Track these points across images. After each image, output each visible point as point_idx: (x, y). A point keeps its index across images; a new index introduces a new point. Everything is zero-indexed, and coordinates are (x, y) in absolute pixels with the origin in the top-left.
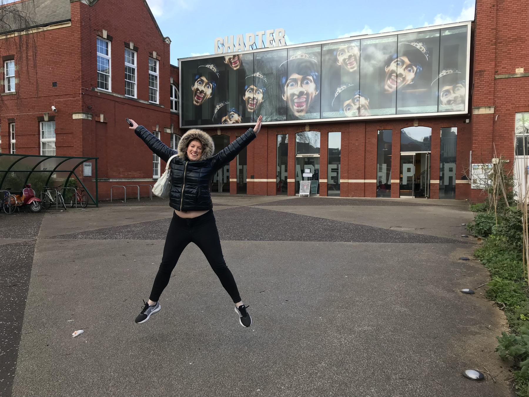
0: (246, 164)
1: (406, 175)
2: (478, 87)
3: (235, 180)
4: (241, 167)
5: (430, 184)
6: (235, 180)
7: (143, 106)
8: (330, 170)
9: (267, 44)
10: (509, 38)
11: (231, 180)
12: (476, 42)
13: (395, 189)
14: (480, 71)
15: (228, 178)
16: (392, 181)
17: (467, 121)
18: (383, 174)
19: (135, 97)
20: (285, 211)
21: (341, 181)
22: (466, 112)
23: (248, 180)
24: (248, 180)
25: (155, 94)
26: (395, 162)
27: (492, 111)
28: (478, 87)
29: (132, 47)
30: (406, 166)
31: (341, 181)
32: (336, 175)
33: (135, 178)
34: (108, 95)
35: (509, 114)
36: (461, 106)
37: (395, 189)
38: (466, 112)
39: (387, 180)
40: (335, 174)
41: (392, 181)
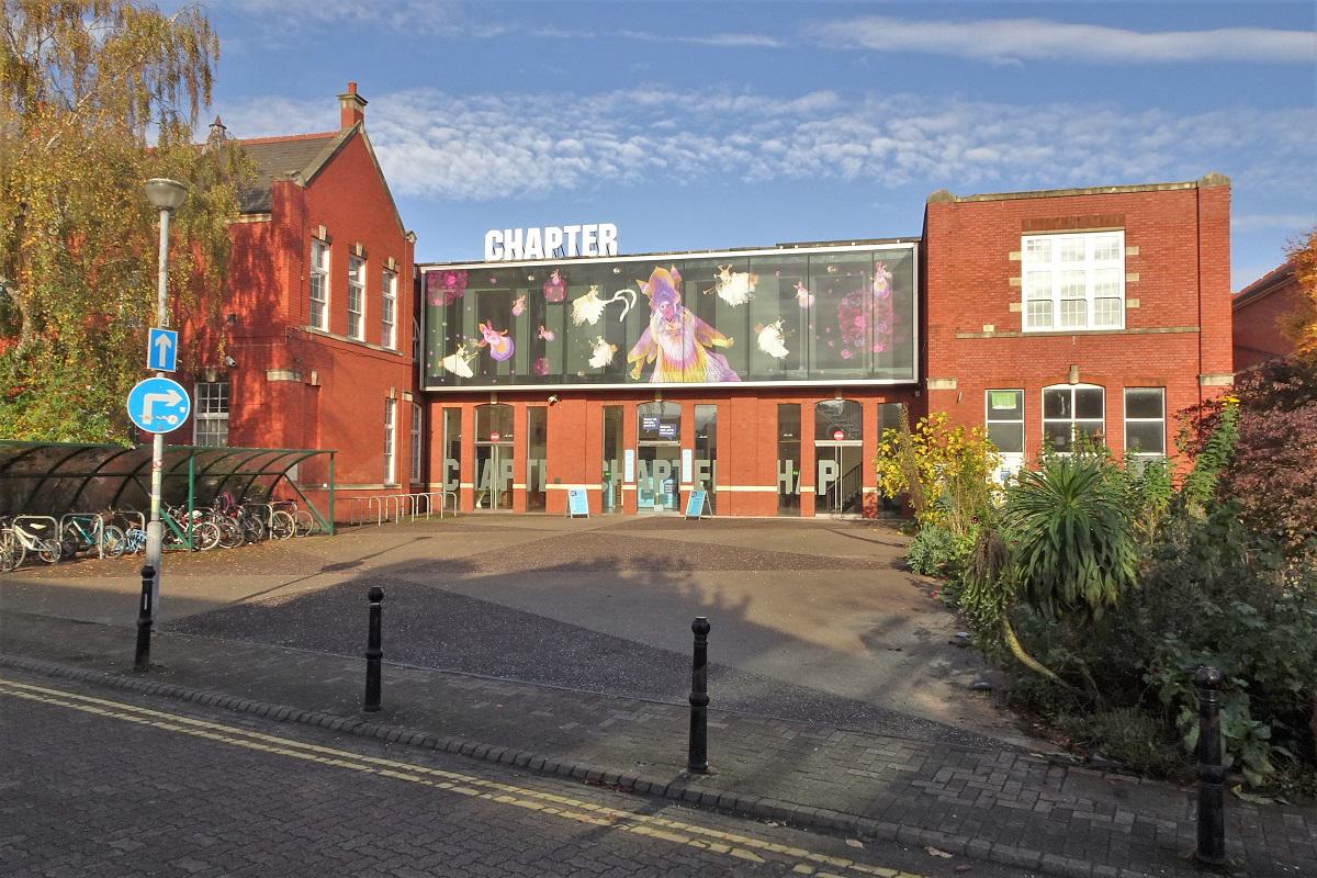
0: (545, 458)
1: (824, 478)
2: (933, 349)
3: (523, 486)
4: (532, 463)
5: (473, 482)
6: (523, 486)
7: (374, 356)
8: (698, 469)
9: (586, 252)
10: (973, 280)
11: (515, 486)
12: (929, 222)
13: (808, 503)
14: (937, 326)
15: (510, 482)
16: (803, 489)
17: (917, 394)
18: (788, 477)
19: (361, 337)
20: (655, 537)
21: (719, 488)
22: (915, 380)
23: (548, 486)
24: (548, 486)
25: (320, 311)
26: (807, 456)
27: (953, 385)
28: (933, 349)
29: (359, 253)
30: (824, 464)
31: (719, 488)
32: (708, 478)
33: (364, 483)
34: (358, 344)
35: (977, 390)
36: (907, 371)
37: (808, 503)
38: (915, 380)
39: (794, 489)
40: (707, 476)
41: (803, 489)
